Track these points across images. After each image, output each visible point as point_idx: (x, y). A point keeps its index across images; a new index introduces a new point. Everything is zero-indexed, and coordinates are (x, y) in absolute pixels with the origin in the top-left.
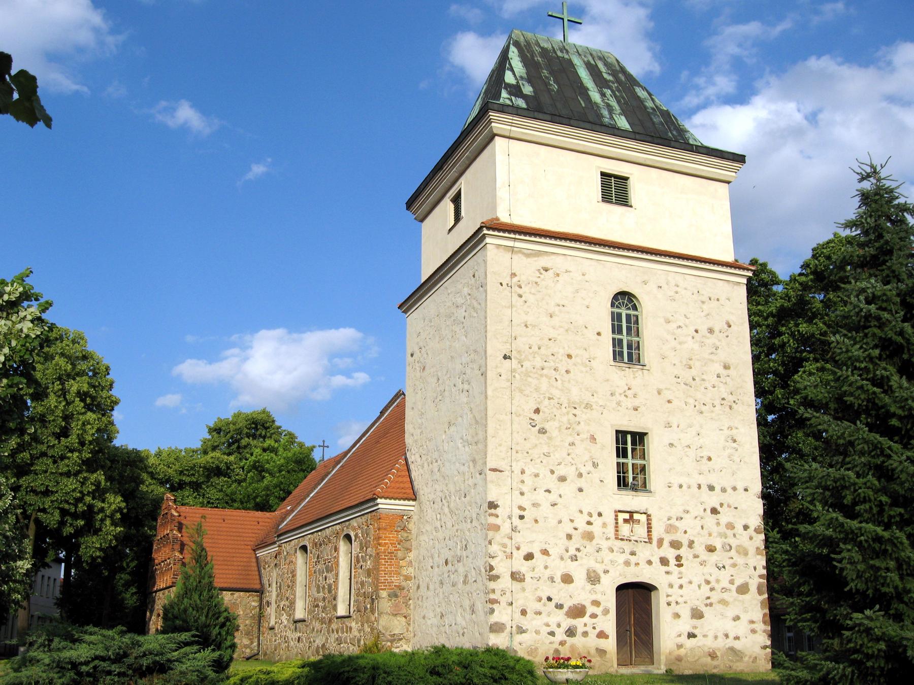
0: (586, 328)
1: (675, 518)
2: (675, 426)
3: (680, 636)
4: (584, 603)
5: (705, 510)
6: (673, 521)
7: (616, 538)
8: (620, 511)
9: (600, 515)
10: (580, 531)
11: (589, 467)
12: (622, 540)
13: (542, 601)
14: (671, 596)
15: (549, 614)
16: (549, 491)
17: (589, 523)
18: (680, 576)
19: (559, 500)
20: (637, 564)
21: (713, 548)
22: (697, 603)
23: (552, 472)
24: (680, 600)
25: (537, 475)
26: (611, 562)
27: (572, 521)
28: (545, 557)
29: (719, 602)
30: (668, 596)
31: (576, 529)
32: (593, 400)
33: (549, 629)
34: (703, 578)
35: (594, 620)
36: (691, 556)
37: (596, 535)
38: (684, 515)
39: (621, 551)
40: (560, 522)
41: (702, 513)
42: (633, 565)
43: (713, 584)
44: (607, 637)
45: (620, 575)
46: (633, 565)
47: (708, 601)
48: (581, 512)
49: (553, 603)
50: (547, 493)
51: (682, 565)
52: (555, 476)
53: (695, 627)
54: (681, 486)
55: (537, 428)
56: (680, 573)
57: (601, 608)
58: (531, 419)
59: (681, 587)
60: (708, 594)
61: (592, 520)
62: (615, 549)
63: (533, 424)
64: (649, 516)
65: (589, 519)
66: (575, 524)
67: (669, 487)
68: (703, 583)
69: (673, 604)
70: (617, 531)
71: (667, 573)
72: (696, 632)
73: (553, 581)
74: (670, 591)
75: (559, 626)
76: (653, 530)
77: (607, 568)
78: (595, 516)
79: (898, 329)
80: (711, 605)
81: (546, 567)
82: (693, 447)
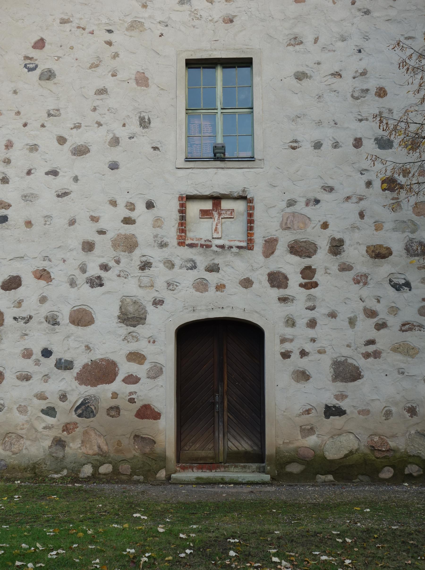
0: (319, 63)
1: (303, 201)
2: (309, 39)
3: (308, 412)
4: (112, 357)
5: (369, 184)
6: (300, 208)
7: (181, 244)
8: (190, 198)
9: (150, 205)
10: (111, 235)
11: (134, 126)
12: (191, 246)
13: (34, 357)
14: (291, 341)
15: (46, 378)
16: (54, 173)
17: (128, 221)
18: (310, 304)
19: (72, 187)
20: (220, 287)
21: (384, 251)
22: (347, 352)
23: (62, 140)
24: (308, 347)
25: (34, 148)
26: (169, 284)
27: (95, 219)
28: (42, 283)
29: (396, 349)
30: (283, 341)
31: (102, 232)
32: (146, 15)
33: (44, 405)
34: (362, 305)
35: (132, 388)
36: (335, 268)
37: (140, 240)
38: (324, 196)
39: (189, 265)
40: (72, 222)
41: (361, 189)
42: (212, 289)
43: (383, 315)
44: (156, 416)
45: (185, 308)
46: (212, 289)
47: (371, 348)
48: (114, 203)
49: (52, 360)
50: (51, 177)
51: (315, 285)
52: (67, 146)
53: (342, 396)
54: (318, 145)
55: (38, 72)
56: (310, 298)
57: (147, 366)
58: (27, 58)
59: (312, 324)
60: (373, 334)
61: (133, 215)
62: (177, 262)
63: (31, 66)
64: (251, 201)
65: (127, 213)
66: (101, 225)
67: (294, 148)
68: (361, 316)
69: (296, 356)
70: (250, 215)
71: (283, 300)
72: (343, 404)
73: (56, 323)
74: (289, 332)
75: (63, 397)
76: (255, 225)
77: (159, 296)
78: (141, 207)
79: (141, 456)
80: (377, 354)
81: (43, 300)
82: (348, 75)
